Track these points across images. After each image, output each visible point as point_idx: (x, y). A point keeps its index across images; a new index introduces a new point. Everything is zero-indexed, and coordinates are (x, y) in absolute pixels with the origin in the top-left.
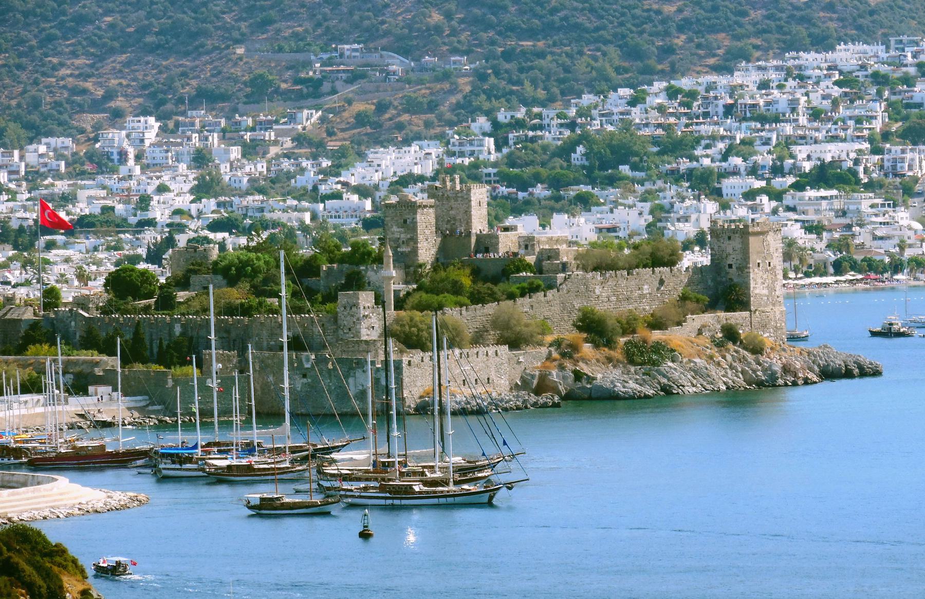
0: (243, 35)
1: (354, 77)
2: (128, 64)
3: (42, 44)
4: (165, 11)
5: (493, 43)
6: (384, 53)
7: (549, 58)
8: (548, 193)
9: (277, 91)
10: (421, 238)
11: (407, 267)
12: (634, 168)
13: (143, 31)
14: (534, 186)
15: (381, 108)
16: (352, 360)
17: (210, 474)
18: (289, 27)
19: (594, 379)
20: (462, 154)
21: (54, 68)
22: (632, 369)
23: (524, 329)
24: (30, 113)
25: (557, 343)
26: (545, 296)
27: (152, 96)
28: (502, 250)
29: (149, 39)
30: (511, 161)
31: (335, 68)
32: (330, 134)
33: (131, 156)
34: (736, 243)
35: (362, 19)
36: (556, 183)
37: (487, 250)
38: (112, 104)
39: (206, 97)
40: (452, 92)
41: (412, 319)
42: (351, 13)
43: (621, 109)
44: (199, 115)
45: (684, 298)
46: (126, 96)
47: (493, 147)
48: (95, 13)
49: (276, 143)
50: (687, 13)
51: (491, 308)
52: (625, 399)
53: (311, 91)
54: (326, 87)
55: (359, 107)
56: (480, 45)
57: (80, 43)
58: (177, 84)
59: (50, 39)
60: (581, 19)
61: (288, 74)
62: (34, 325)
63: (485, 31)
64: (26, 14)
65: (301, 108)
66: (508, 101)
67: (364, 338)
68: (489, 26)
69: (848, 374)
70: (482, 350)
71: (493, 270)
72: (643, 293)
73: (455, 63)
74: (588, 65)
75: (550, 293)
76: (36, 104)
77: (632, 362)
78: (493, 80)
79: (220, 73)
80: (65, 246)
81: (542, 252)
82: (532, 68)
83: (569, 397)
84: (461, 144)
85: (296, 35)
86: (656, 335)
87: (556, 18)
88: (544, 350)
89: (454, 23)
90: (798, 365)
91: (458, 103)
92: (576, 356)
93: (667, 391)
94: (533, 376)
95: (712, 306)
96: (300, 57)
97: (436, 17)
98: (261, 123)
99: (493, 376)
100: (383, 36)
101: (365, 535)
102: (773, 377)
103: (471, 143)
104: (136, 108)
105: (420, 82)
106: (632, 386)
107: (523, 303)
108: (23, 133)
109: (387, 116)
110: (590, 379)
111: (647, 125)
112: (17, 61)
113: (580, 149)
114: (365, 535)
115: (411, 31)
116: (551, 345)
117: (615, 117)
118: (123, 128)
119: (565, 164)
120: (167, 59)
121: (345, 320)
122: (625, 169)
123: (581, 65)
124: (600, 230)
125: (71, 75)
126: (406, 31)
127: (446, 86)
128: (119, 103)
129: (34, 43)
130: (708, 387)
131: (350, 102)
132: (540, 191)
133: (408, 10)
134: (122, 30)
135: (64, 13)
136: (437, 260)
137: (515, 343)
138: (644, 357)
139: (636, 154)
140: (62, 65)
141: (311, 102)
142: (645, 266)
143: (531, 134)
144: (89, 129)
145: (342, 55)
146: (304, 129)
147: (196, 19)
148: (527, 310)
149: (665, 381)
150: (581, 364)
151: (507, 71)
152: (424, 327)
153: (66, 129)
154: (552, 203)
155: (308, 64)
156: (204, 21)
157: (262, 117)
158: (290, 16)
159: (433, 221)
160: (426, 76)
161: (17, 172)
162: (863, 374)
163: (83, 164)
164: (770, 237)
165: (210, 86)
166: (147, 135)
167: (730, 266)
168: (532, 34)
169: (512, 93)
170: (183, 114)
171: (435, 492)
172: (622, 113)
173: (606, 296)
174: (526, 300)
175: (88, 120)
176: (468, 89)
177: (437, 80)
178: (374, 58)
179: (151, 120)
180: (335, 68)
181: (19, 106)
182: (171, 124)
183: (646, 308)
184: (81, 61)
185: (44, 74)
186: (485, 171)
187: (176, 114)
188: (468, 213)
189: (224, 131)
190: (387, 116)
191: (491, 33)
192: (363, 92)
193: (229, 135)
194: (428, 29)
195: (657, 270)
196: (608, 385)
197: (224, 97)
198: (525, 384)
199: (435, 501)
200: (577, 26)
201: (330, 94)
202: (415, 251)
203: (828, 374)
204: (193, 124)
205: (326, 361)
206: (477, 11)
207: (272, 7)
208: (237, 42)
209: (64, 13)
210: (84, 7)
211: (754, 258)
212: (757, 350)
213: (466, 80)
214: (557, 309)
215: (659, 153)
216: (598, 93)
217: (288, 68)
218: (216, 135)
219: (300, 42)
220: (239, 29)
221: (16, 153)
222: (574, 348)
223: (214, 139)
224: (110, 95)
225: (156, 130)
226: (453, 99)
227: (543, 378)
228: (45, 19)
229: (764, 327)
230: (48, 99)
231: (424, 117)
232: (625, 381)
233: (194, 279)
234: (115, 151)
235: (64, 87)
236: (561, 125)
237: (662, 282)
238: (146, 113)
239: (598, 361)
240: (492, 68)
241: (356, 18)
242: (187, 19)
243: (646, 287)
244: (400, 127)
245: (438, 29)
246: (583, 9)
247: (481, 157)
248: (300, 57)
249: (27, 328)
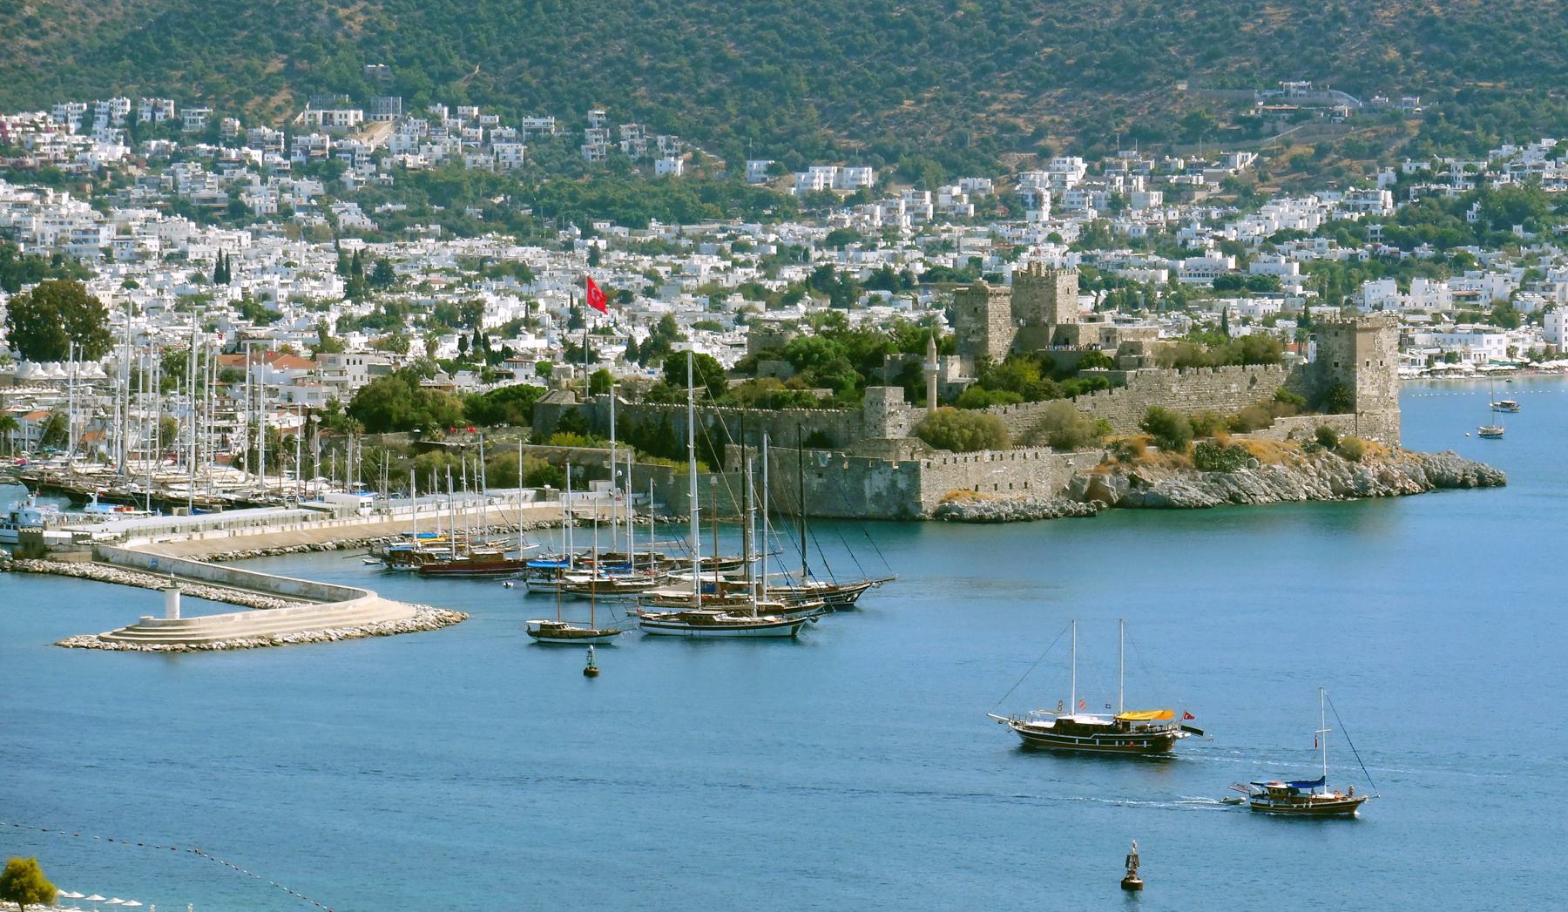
0: (1187, 69)
1: (1297, 118)
2: (1062, 99)
3: (975, 77)
4: (1108, 42)
5: (1449, 83)
6: (1334, 92)
7: (1508, 100)
8: (1431, 253)
9: (1215, 131)
10: (991, 327)
11: (976, 358)
12: (1527, 228)
13: (1083, 64)
14: (1419, 245)
15: (1321, 152)
16: (867, 461)
17: (569, 591)
18: (1236, 62)
19: (1151, 485)
20: (1356, 209)
21: (986, 103)
22: (1200, 475)
23: (1075, 429)
24: (954, 149)
25: (1116, 446)
27: (1085, 134)
28: (1083, 342)
29: (1087, 73)
30: (1403, 218)
31: (1277, 107)
32: (1263, 179)
34: (1343, 340)
35: (1314, 53)
36: (1442, 243)
37: (1067, 342)
38: (1042, 143)
39: (1141, 137)
40: (1399, 135)
41: (943, 417)
42: (1302, 47)
43: (1534, 162)
44: (1130, 156)
45: (1279, 398)
46: (1057, 134)
47: (1390, 200)
48: (1035, 44)
49: (1203, 188)
51: (1044, 406)
52: (1179, 508)
53: (1249, 132)
54: (1267, 127)
55: (1297, 150)
56: (1435, 85)
57: (1015, 76)
58: (1112, 122)
59: (985, 70)
60: (1548, 59)
61: (1228, 113)
62: (571, 411)
63: (1442, 70)
64: (962, 44)
65: (1236, 150)
66: (1456, 147)
67: (889, 437)
68: (1447, 64)
69: (1464, 485)
70: (1030, 453)
71: (1065, 364)
72: (1232, 391)
73: (1406, 103)
74: (1549, 109)
75: (1116, 391)
76: (961, 141)
77: (1200, 467)
78: (1443, 123)
79: (1157, 110)
80: (890, 302)
81: (1124, 345)
82: (1487, 111)
83: (1123, 504)
84: (1356, 197)
85: (1241, 71)
86: (1237, 438)
87: (1520, 57)
88: (1099, 453)
89: (1410, 60)
90: (1397, 474)
91: (1403, 147)
93: (1235, 498)
94: (1084, 481)
95: (1313, 406)
96: (1243, 94)
97: (1392, 54)
98: (1192, 165)
99: (1031, 480)
100: (1333, 74)
101: (590, 673)
102: (1364, 486)
103: (1365, 196)
104: (1065, 147)
105: (1367, 124)
106: (1194, 493)
107: (1085, 402)
108: (942, 172)
109: (1327, 161)
110: (1147, 485)
111: (1557, 180)
112: (948, 94)
114: (590, 673)
115: (1363, 68)
116: (1108, 447)
117: (1527, 171)
118: (1048, 169)
119: (1459, 221)
120: (1104, 94)
121: (870, 417)
122: (1518, 230)
123: (1541, 110)
124: (1458, 298)
125: (1003, 110)
126: (1358, 68)
127: (1394, 129)
128: (1050, 141)
129: (967, 75)
130: (1286, 496)
131: (1288, 144)
132: (1425, 251)
133: (1363, 46)
134: (1062, 64)
135: (1002, 43)
136: (1012, 351)
137: (1063, 444)
138: (1216, 462)
139: (1532, 213)
140: (994, 99)
141: (1250, 143)
142: (1236, 363)
143: (1434, 187)
144: (1014, 169)
145: (1287, 93)
146: (1236, 172)
147: (1140, 52)
148: (1084, 409)
149: (1234, 489)
150: (1140, 469)
151: (1460, 114)
152: (955, 426)
153: (989, 169)
154: (1431, 264)
155: (1251, 102)
156: (1147, 54)
157: (1194, 159)
158: (1239, 50)
159: (1009, 310)
160: (1373, 118)
161: (924, 215)
162: (1483, 483)
163: (994, 208)
164: (1383, 334)
165: (1144, 124)
166: (1069, 177)
167: (1336, 365)
168: (1492, 74)
169: (1463, 137)
170: (1115, 154)
173: (1182, 397)
174: (1089, 397)
175: (1013, 159)
176: (1416, 132)
177: (1385, 122)
178: (1322, 97)
179: (1078, 161)
180: (1277, 107)
181: (944, 143)
182: (1097, 165)
183: (1234, 408)
184: (1016, 95)
185: (974, 109)
186: (1372, 227)
187: (1108, 155)
188: (1053, 301)
189: (1151, 173)
190: (1327, 161)
191: (1449, 73)
192: (1303, 134)
193: (1154, 181)
194: (1383, 67)
195: (1248, 367)
196: (1165, 493)
197: (1158, 137)
198: (1073, 492)
199: (743, 632)
200: (1542, 67)
201: (1268, 135)
202: (985, 342)
203: (1442, 484)
204: (1119, 166)
205: (842, 460)
206: (1435, 48)
207: (1221, 39)
208: (1182, 77)
209: (1002, 43)
210: (1023, 37)
211: (1361, 356)
212: (1353, 456)
213: (1417, 122)
214: (1124, 408)
215: (1555, 213)
216: (1518, 144)
217: (1229, 107)
218: (1141, 178)
219: (1246, 80)
220: (1183, 62)
221: (928, 194)
222: (1134, 451)
223: (1140, 182)
224: (1040, 133)
226: (1399, 143)
227: (1095, 483)
228: (982, 49)
229: (1372, 430)
230: (975, 135)
231: (1365, 162)
232: (1187, 487)
233: (761, 365)
234: (1030, 194)
235: (994, 123)
236: (1468, 178)
237: (1253, 381)
238: (1073, 152)
239: (1162, 465)
240: (1444, 110)
241: (1306, 53)
242: (1129, 50)
244: (1338, 173)
245: (1392, 68)
246: (1550, 48)
247: (1374, 212)
248: (1243, 94)
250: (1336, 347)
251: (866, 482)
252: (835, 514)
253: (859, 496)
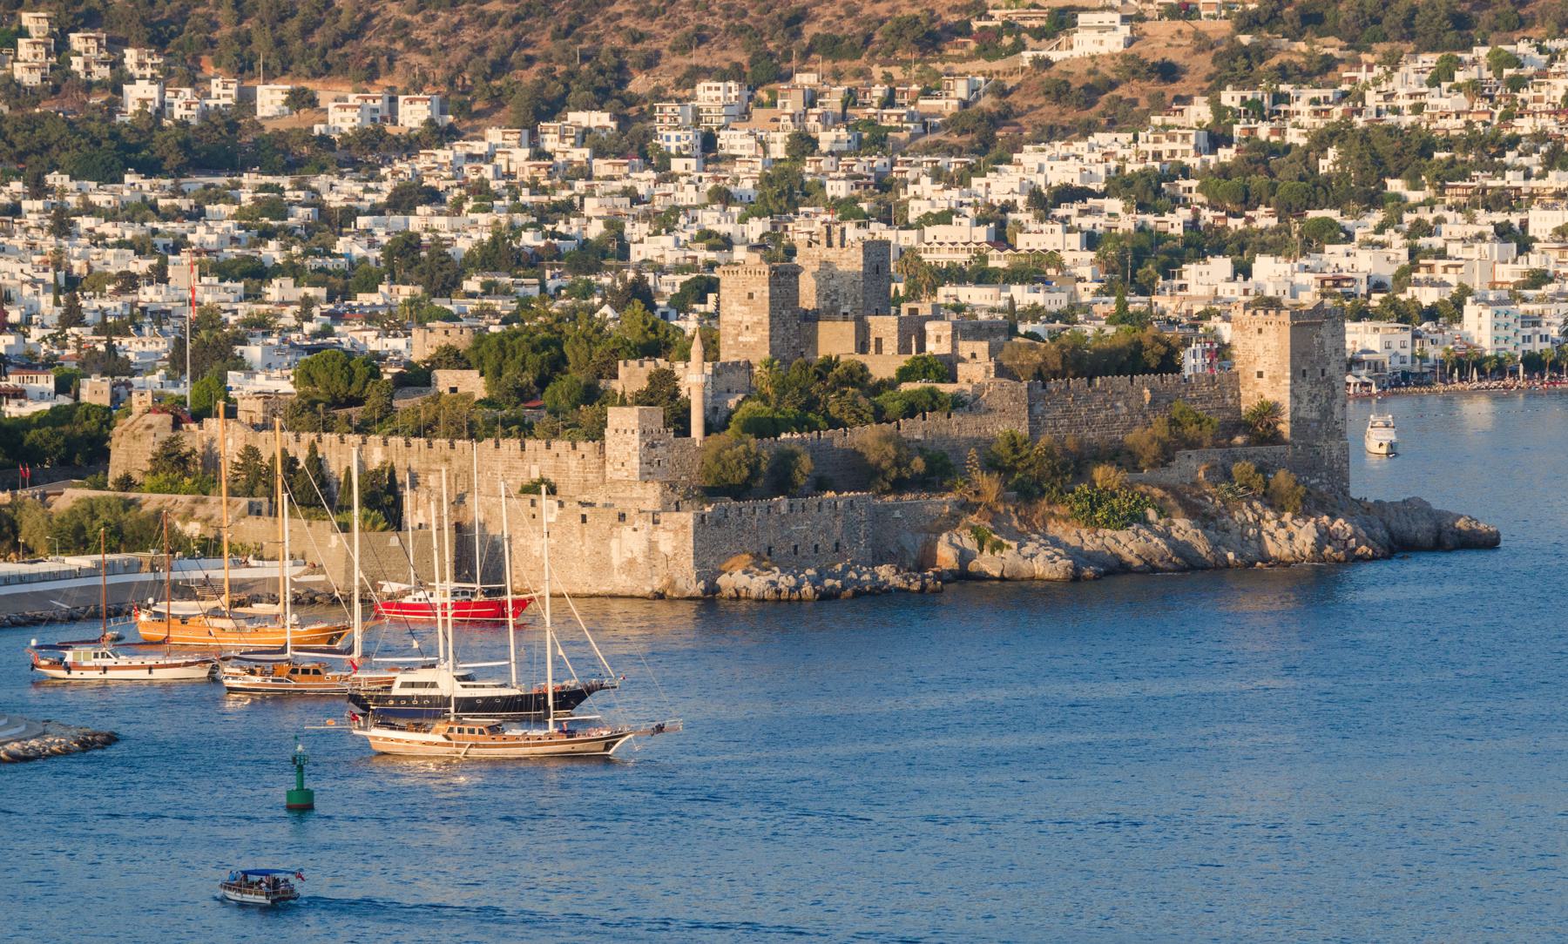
113: (1332, 152)
122: (1395, 185)
125: (628, 12)
132: (1264, 218)
167: (1260, 375)
172: (1411, 96)
250: (1259, 349)
251: (614, 544)
252: (586, 590)
253: (602, 566)
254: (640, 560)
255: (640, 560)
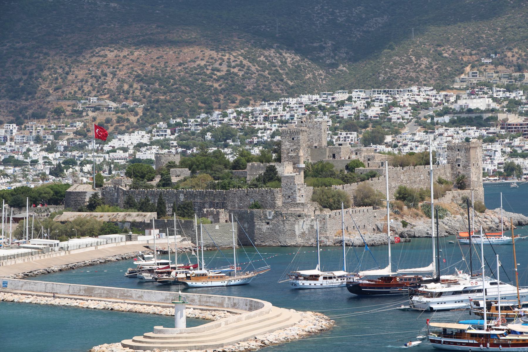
26: (379, 179)
33: (9, 139)
50: (223, 86)
54: (84, 114)
92: (401, 213)
141: (79, 119)
142: (421, 165)
171: (388, 292)
182: (23, 126)
211: (472, 161)
225: (17, 129)
238: (11, 122)
243: (422, 176)
249: (91, 196)
254: (307, 232)
255: (307, 232)
